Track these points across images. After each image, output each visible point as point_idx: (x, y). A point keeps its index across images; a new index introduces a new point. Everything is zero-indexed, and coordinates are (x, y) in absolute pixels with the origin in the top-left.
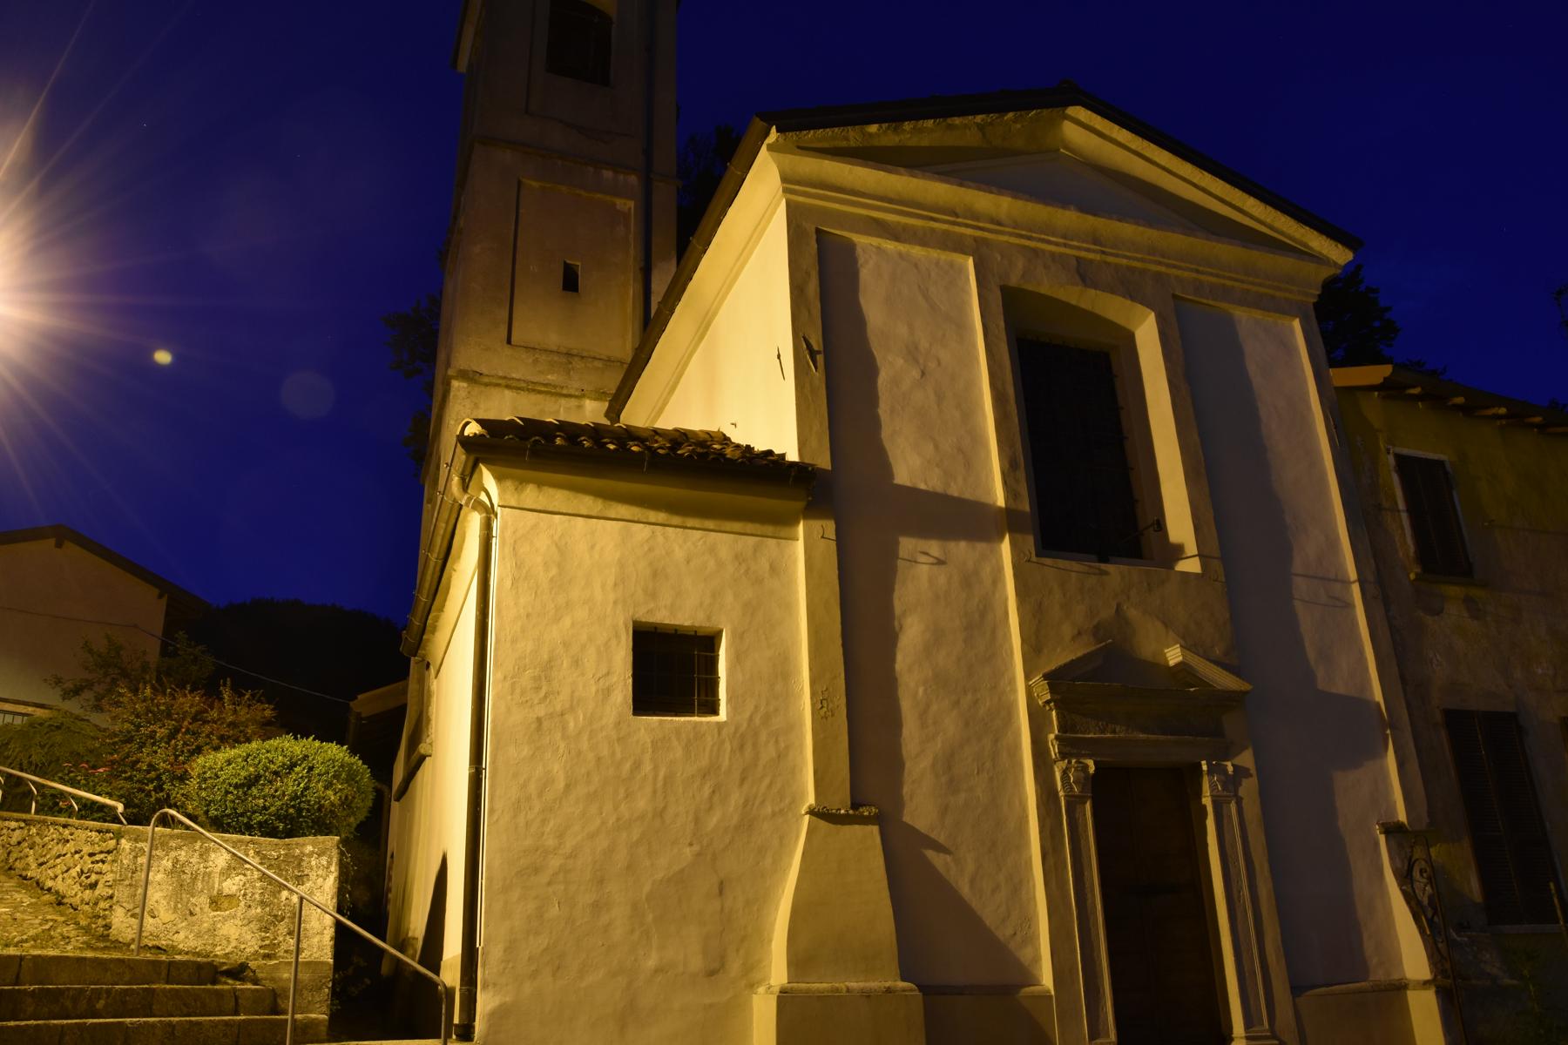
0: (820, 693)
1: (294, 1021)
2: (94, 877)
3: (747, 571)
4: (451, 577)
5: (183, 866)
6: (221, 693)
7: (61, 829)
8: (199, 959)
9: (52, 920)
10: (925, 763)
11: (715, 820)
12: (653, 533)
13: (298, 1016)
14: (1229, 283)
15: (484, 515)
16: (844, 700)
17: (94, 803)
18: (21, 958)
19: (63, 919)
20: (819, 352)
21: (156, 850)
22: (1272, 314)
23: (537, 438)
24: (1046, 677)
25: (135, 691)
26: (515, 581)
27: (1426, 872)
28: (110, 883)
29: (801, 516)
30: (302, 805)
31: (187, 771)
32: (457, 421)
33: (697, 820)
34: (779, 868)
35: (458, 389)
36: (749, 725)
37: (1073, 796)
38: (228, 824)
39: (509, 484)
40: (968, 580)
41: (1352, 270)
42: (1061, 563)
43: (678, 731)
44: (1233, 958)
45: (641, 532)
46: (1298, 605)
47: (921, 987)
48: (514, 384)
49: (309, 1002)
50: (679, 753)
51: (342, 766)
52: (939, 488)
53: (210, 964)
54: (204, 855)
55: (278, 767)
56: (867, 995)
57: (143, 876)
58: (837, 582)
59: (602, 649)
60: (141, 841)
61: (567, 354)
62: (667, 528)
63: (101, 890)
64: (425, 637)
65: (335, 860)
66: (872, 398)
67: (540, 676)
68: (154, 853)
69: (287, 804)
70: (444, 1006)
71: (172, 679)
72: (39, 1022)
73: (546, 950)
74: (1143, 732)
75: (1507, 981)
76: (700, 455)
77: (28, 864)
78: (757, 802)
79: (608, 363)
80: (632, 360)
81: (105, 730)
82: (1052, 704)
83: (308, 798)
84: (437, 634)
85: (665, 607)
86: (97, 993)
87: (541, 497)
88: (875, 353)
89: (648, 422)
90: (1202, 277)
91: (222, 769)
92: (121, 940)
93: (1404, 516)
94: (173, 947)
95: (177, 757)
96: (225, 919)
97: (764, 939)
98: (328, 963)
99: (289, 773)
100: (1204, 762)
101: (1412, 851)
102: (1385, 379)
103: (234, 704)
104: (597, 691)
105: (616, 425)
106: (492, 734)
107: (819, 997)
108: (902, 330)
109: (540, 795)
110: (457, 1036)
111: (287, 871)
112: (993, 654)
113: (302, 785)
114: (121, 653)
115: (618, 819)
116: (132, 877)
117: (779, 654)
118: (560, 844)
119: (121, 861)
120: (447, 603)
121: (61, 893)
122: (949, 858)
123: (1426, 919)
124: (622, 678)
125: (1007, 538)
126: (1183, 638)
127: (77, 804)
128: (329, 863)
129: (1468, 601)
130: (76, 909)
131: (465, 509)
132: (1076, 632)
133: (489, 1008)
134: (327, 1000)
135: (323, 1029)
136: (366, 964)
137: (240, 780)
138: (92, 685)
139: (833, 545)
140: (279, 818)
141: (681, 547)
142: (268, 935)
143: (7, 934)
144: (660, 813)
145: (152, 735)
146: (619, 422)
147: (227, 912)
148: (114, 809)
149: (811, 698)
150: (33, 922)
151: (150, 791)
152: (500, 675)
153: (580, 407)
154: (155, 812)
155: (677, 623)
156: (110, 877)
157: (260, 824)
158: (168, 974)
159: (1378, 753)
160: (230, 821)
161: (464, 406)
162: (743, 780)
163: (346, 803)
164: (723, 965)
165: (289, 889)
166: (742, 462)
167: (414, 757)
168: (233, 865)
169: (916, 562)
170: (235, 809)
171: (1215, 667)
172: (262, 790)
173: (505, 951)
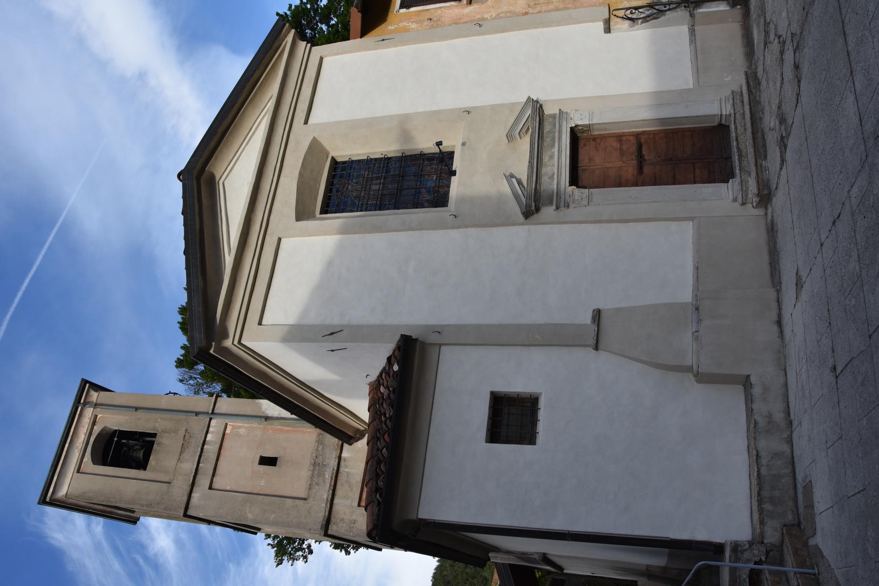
27: (632, 11)
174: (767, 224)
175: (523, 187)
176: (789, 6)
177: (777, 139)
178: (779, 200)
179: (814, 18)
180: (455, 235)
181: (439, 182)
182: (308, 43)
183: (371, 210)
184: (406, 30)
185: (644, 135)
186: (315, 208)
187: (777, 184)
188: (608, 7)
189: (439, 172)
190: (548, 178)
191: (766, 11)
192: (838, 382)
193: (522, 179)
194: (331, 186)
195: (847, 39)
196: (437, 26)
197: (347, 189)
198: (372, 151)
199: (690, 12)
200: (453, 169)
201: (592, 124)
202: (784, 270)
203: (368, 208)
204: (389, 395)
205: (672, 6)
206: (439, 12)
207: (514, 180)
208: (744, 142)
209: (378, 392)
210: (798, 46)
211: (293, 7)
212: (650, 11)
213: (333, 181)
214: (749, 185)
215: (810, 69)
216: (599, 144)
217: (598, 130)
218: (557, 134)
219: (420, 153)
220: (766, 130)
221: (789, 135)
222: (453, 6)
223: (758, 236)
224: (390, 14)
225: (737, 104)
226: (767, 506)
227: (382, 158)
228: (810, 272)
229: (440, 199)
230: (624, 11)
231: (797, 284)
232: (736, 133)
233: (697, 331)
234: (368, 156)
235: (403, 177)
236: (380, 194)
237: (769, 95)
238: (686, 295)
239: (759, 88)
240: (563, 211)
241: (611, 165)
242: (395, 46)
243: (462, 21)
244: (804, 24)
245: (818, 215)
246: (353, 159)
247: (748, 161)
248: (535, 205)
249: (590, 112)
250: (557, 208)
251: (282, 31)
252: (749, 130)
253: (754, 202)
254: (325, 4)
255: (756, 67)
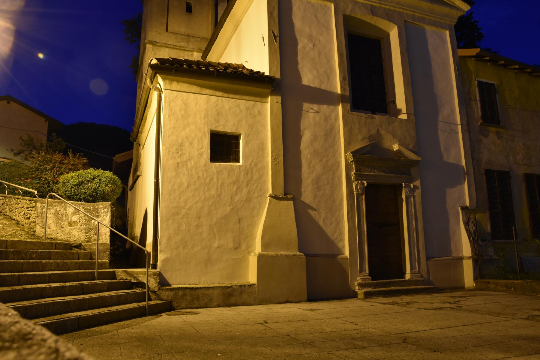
0: (274, 156)
1: (98, 262)
2: (29, 216)
3: (250, 114)
4: (147, 114)
5: (58, 212)
6: (68, 154)
7: (16, 200)
8: (65, 242)
9: (16, 229)
10: (309, 181)
11: (238, 198)
12: (218, 99)
13: (99, 261)
14: (425, 16)
15: (159, 92)
16: (282, 159)
17: (27, 191)
18: (7, 241)
19: (19, 229)
20: (277, 37)
21: (49, 206)
22: (439, 28)
23: (177, 65)
24: (352, 153)
25: (39, 154)
26: (169, 115)
27: (474, 222)
28: (34, 217)
29: (270, 95)
30: (98, 192)
31: (58, 180)
32: (149, 59)
33: (232, 198)
34: (259, 214)
35: (149, 48)
36: (250, 167)
37: (358, 193)
38: (73, 198)
39: (167, 81)
40: (327, 119)
41: (469, 13)
42: (359, 114)
43: (225, 168)
44: (408, 248)
45: (213, 99)
46: (439, 131)
47: (305, 255)
48: (169, 46)
49: (102, 256)
50: (226, 175)
51: (111, 179)
52: (318, 87)
53: (69, 244)
54: (65, 208)
55: (89, 179)
56: (287, 256)
57: (45, 215)
58: (281, 118)
59: (200, 139)
60: (44, 204)
61: (188, 35)
62: (223, 98)
63: (31, 220)
64: (138, 135)
65: (109, 210)
66: (296, 54)
67: (178, 149)
68: (48, 207)
69: (93, 192)
70: (147, 258)
71: (51, 149)
72: (15, 261)
73: (181, 240)
74: (384, 173)
75: (495, 257)
76: (234, 72)
77: (6, 211)
78: (252, 192)
79: (203, 39)
80: (211, 38)
81: (29, 167)
82: (353, 162)
83: (100, 189)
84: (142, 134)
85: (222, 125)
86: (33, 252)
87: (178, 86)
88: (297, 37)
89: (217, 60)
90: (415, 14)
91: (70, 180)
92: (39, 236)
93: (479, 103)
94: (56, 238)
95: (54, 176)
96: (73, 229)
97: (253, 238)
98: (108, 244)
99: (93, 181)
100: (403, 184)
101: (470, 216)
102: (477, 53)
103: (73, 158)
104: (198, 154)
105: (205, 61)
106: (162, 168)
107: (271, 257)
108: (307, 29)
109: (179, 189)
110: (151, 267)
111: (93, 213)
112: (334, 144)
113: (97, 185)
114: (33, 140)
115: (205, 197)
116: (41, 216)
117: (261, 142)
118: (185, 205)
119: (38, 210)
120: (146, 123)
121: (18, 221)
122: (316, 213)
123: (472, 238)
124: (207, 150)
125: (341, 103)
126: (399, 141)
127: (21, 191)
128: (108, 211)
129: (498, 133)
130: (23, 226)
131: (152, 90)
132: (363, 138)
133: (162, 258)
134: (108, 256)
135: (108, 265)
136: (121, 244)
137: (76, 183)
138: (24, 151)
139: (280, 105)
140: (90, 196)
141: (227, 104)
142: (88, 234)
143: (1, 233)
144: (219, 196)
145: (46, 168)
146: (206, 60)
147: (74, 227)
148: (34, 193)
149: (271, 158)
150: (10, 230)
151: (46, 187)
152: (165, 148)
153: (192, 55)
154: (48, 194)
155: (226, 131)
156: (34, 215)
157: (84, 198)
158: (55, 247)
159: (462, 183)
160: (73, 197)
161: (151, 54)
162: (247, 185)
163: (113, 191)
164: (240, 246)
165: (94, 220)
166: (249, 75)
167: (136, 176)
168: (75, 212)
169: (309, 112)
170: (75, 193)
171: (410, 152)
172: (84, 187)
173: (167, 240)
192: (258, 324)
195: (462, 327)
226: (181, 293)
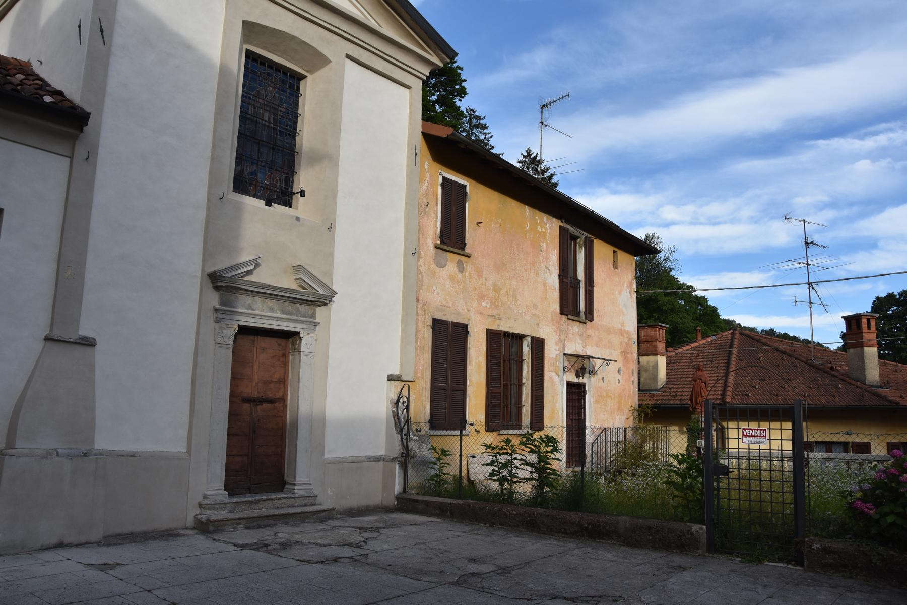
27: (406, 403)
174: (176, 529)
175: (243, 276)
176: (392, 551)
177: (266, 540)
178: (201, 542)
179: (381, 576)
180: (201, 195)
181: (261, 187)
182: (427, 77)
183: (242, 106)
184: (422, 180)
185: (283, 406)
186: (254, 45)
187: (219, 540)
188: (413, 380)
189: (271, 188)
190: (250, 304)
191: (390, 529)
193: (252, 276)
194: (275, 68)
196: (420, 211)
197: (270, 85)
198: (306, 121)
199: (397, 457)
200: (272, 204)
201: (300, 355)
202: (123, 549)
203: (244, 104)
204: (10, 83)
205: (405, 441)
206: (433, 215)
207: (253, 267)
208: (264, 506)
209: (17, 71)
210: (356, 560)
211: (459, 71)
212: (403, 420)
213: (280, 71)
214: (220, 511)
215: (333, 573)
216: (279, 360)
217: (294, 359)
218: (295, 317)
219: (295, 171)
220: (275, 529)
221: (269, 553)
222: (436, 230)
223: (163, 521)
224: (439, 166)
225: (303, 500)
227: (297, 130)
228: (119, 579)
229: (242, 185)
230: (407, 395)
231: (105, 564)
232: (275, 499)
233: (58, 455)
234: (300, 115)
235: (273, 149)
236: (258, 120)
237: (310, 532)
238: (102, 443)
239: (317, 522)
240: (212, 316)
241: (255, 370)
242: (408, 166)
243: (421, 237)
244: (375, 566)
245: (183, 586)
246: (300, 98)
247: (245, 510)
248: (222, 287)
249: (312, 354)
250: (216, 310)
251: (443, 53)
252: (277, 512)
253: (201, 516)
254: (456, 104)
255: (338, 519)
